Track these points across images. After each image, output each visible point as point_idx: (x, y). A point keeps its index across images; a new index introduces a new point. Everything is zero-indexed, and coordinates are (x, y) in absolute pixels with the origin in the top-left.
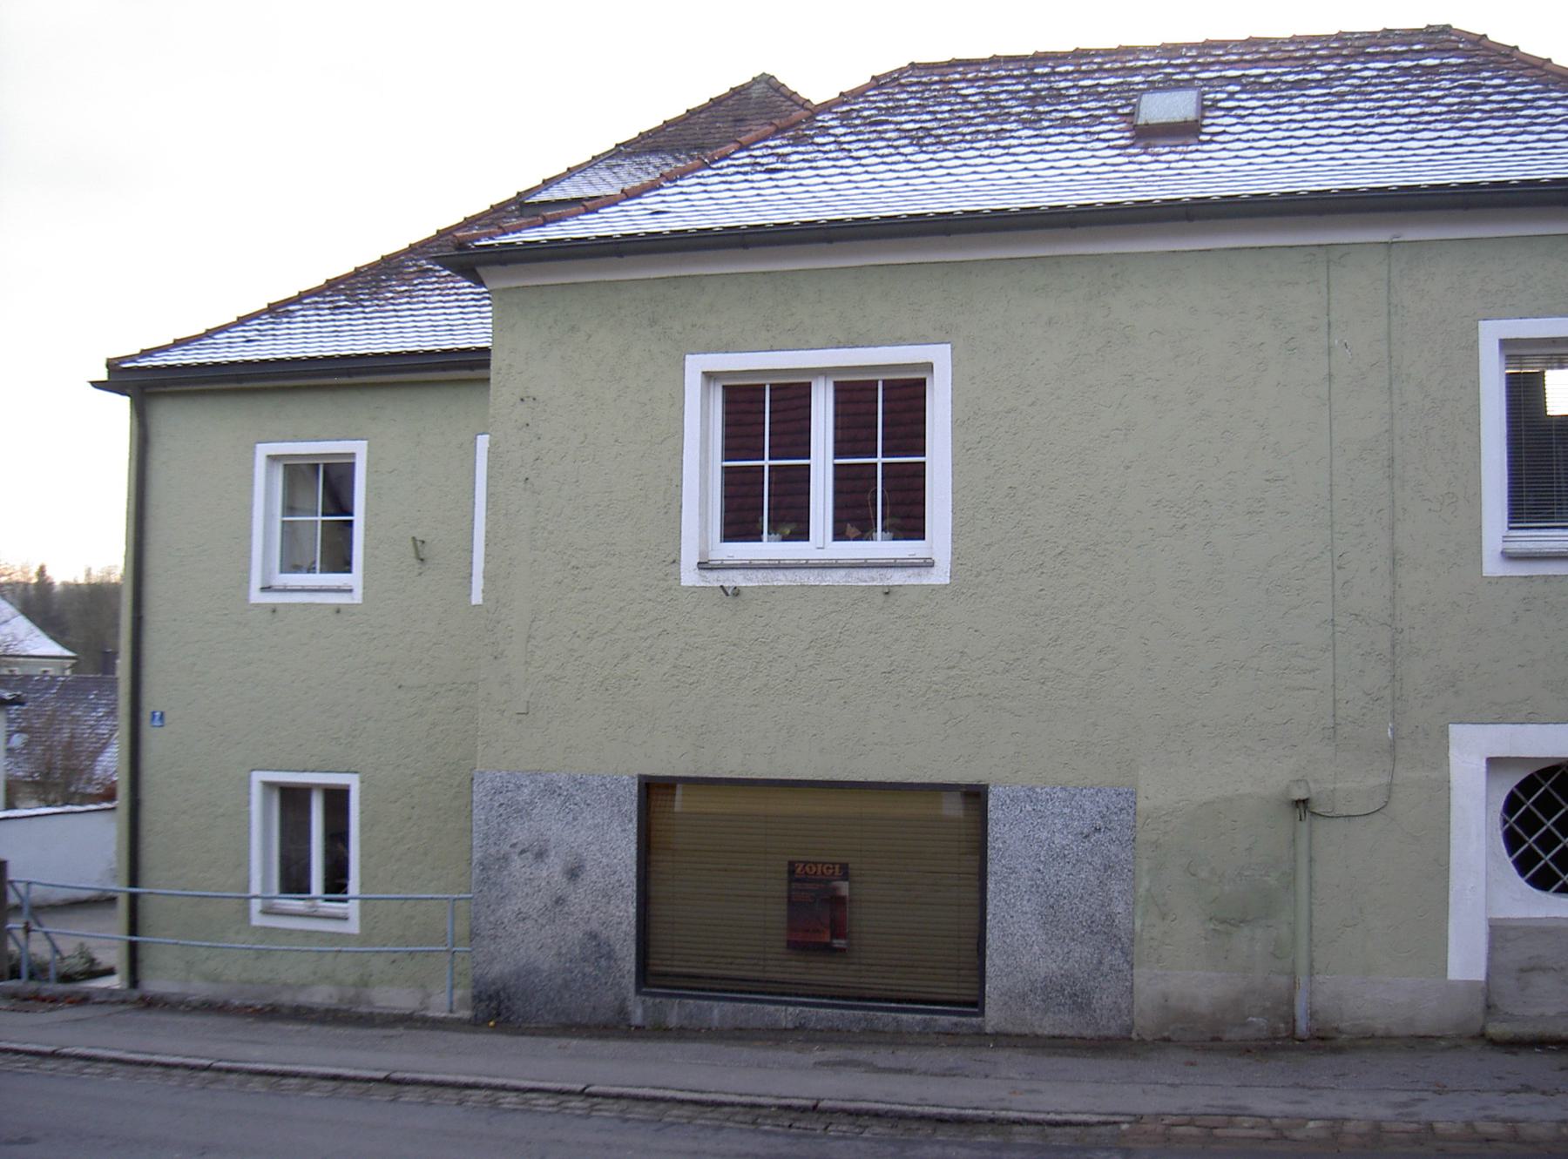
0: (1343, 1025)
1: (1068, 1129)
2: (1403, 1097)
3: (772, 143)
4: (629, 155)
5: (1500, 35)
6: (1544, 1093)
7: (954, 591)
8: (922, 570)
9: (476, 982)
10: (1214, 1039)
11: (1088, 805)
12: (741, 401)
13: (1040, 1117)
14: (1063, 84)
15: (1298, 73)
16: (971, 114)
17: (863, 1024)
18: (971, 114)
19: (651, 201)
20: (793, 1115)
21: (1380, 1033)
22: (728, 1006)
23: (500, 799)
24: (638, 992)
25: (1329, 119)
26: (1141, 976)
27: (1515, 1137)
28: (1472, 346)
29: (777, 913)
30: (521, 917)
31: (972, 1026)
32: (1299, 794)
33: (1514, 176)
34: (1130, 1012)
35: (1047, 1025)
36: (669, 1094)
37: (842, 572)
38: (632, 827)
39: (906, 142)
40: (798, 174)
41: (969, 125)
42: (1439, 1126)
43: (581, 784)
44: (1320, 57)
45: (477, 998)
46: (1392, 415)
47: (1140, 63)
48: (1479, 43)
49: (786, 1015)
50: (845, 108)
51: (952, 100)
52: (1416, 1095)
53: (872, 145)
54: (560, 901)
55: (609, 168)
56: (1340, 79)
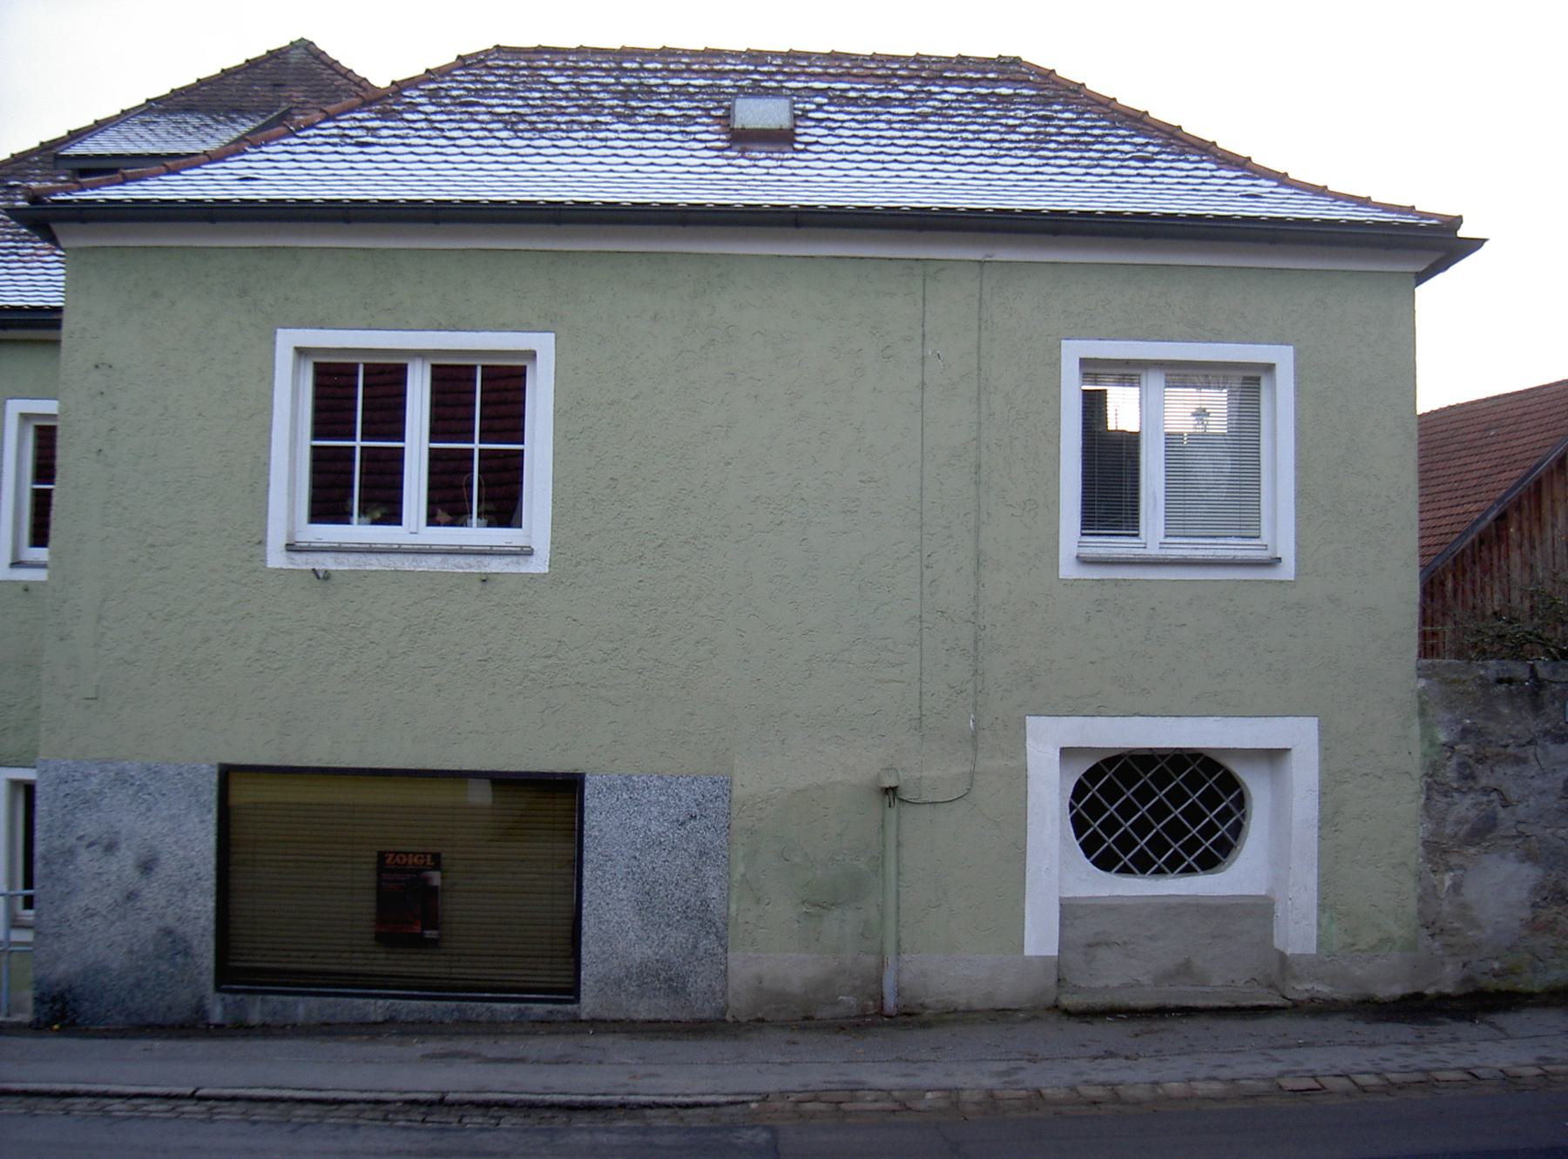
0: (928, 1001)
1: (698, 1111)
2: (1003, 1066)
3: (359, 116)
4: (162, 113)
5: (1068, 71)
6: (1127, 1058)
7: (554, 579)
8: (521, 559)
9: (38, 983)
10: (806, 1018)
11: (683, 793)
12: (333, 383)
13: (670, 1099)
14: (653, 81)
15: (881, 91)
16: (564, 103)
17: (456, 1015)
18: (564, 103)
19: (235, 164)
20: (423, 1109)
21: (961, 1008)
22: (314, 1002)
23: (65, 789)
24: (218, 989)
25: (916, 138)
26: (735, 960)
27: (1117, 1099)
28: (1054, 365)
29: (366, 905)
30: (90, 913)
31: (568, 1013)
32: (889, 782)
33: (1099, 206)
34: (724, 994)
35: (643, 1010)
36: (287, 1093)
37: (438, 558)
38: (212, 818)
39: (500, 126)
40: (390, 149)
41: (563, 114)
42: (1047, 1092)
43: (155, 772)
44: (901, 77)
45: (39, 1000)
46: (980, 424)
47: (728, 67)
48: (1047, 77)
49: (375, 1008)
50: (432, 86)
51: (543, 87)
52: (1013, 1064)
53: (466, 126)
54: (132, 896)
55: (144, 124)
56: (921, 100)
